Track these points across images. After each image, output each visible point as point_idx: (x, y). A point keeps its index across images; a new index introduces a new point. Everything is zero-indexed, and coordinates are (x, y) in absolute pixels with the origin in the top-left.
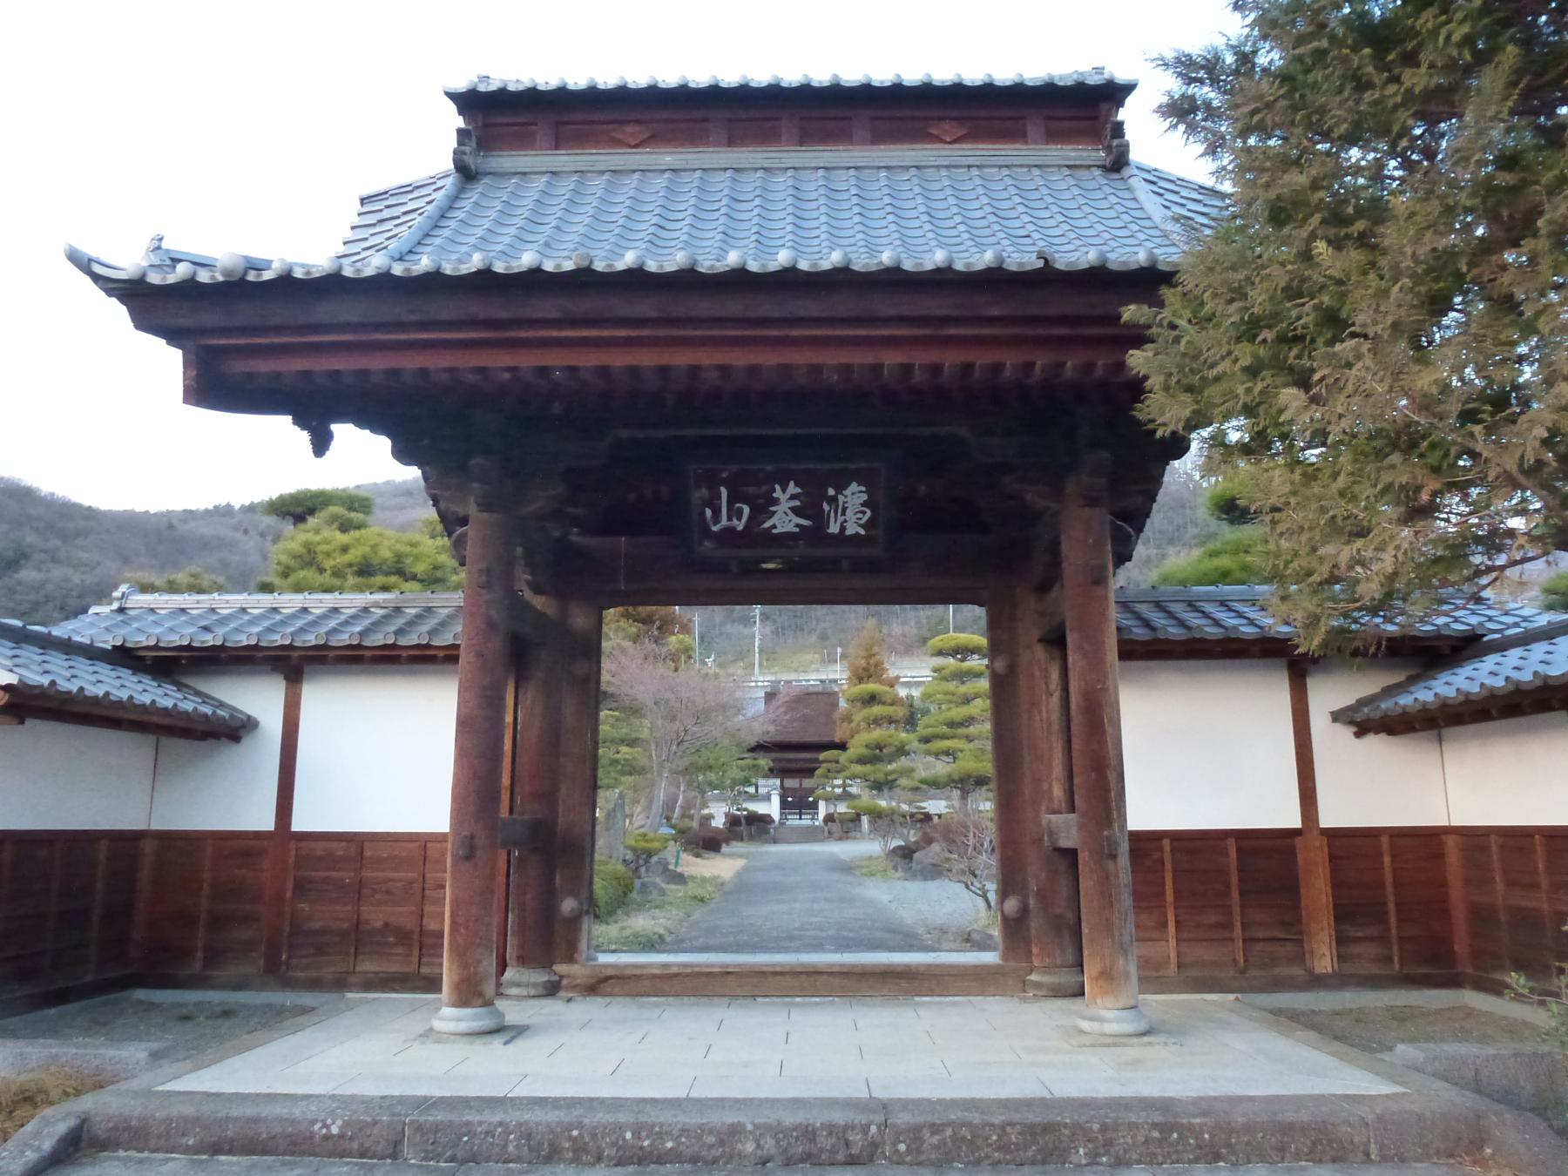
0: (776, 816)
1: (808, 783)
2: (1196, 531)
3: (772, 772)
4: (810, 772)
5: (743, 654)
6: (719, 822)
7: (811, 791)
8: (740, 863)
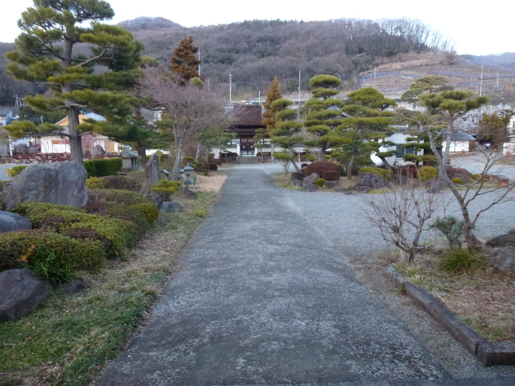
0: (239, 153)
1: (250, 140)
2: (386, 50)
3: (237, 137)
4: (252, 136)
5: (226, 94)
6: (217, 156)
7: (252, 144)
8: (224, 178)
